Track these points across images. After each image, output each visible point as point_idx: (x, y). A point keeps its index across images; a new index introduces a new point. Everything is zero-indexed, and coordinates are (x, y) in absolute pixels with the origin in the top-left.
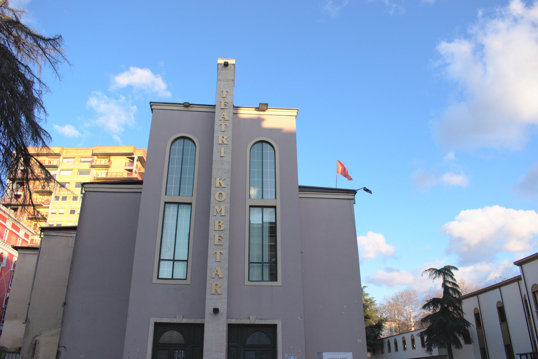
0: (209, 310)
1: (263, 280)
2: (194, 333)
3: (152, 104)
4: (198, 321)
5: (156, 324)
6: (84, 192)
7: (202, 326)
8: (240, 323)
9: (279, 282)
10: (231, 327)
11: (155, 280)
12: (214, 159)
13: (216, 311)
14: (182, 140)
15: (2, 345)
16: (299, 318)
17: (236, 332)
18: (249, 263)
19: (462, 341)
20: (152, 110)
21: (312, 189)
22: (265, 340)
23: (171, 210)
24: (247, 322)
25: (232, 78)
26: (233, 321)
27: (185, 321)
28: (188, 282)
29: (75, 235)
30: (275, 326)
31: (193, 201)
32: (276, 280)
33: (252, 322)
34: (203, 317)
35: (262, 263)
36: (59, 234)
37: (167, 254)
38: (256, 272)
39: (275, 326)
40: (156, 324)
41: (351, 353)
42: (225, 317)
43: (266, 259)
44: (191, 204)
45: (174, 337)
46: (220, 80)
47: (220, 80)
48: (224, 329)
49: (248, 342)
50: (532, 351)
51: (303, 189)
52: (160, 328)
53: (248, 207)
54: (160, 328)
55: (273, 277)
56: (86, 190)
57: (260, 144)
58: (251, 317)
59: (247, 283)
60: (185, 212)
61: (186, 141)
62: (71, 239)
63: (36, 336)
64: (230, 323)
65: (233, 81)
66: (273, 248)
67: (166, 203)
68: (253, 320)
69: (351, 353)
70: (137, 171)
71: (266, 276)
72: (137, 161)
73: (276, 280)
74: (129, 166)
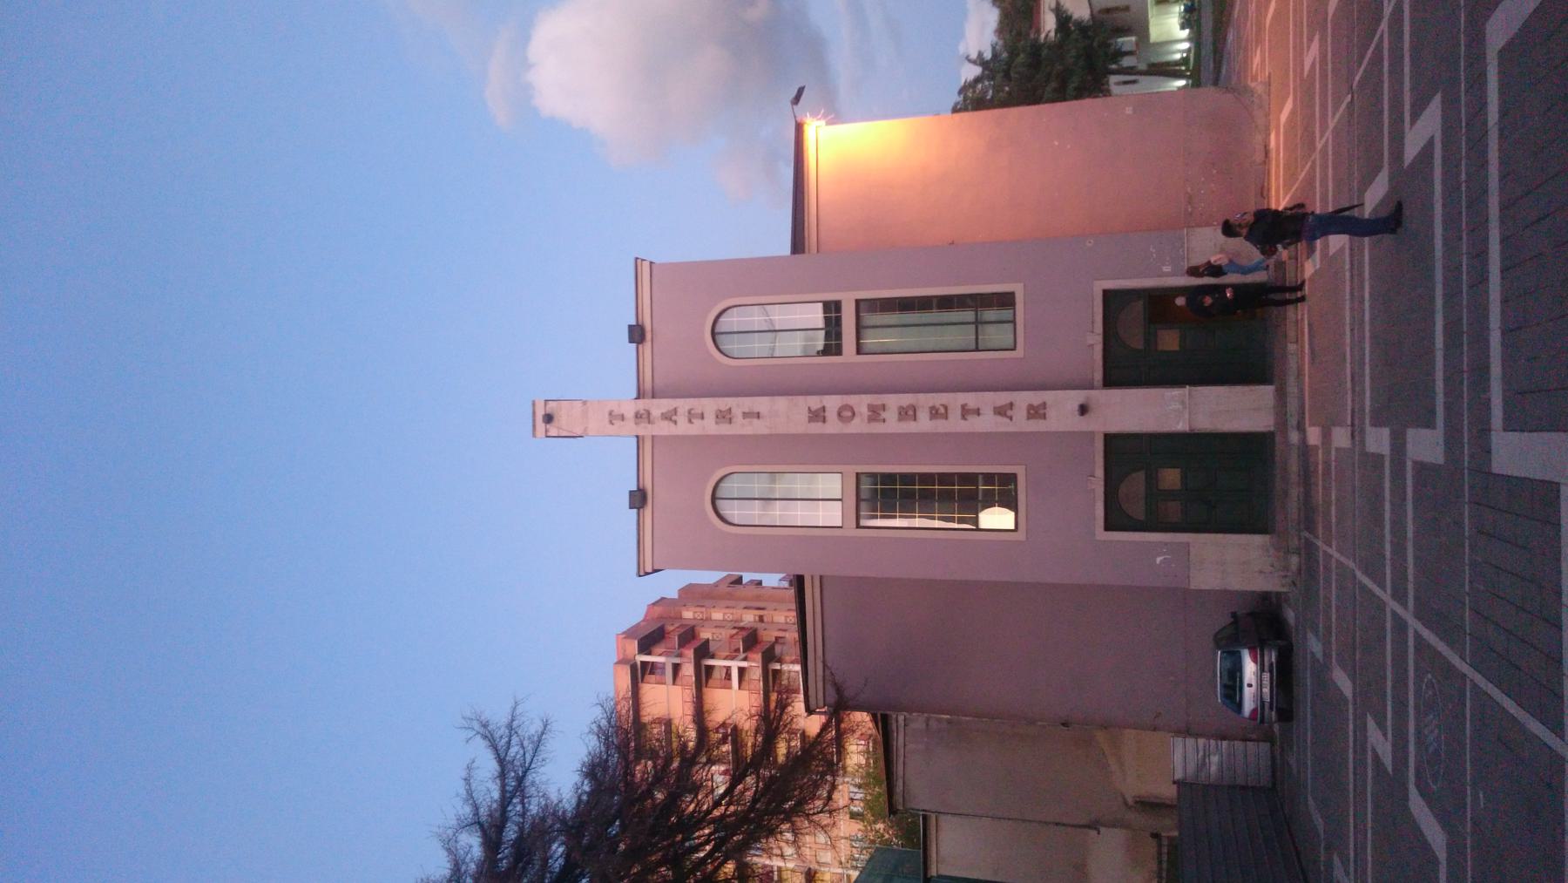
1: (1014, 322)
2: (1124, 453)
4: (1099, 445)
5: (1109, 527)
7: (1109, 439)
9: (1017, 289)
10: (1109, 382)
13: (1083, 409)
14: (720, 503)
17: (1123, 369)
18: (977, 350)
19: (1299, 294)
20: (655, 571)
24: (1099, 349)
25: (579, 404)
26: (1098, 376)
27: (1100, 472)
30: (1107, 294)
35: (977, 323)
36: (900, 773)
38: (996, 335)
39: (1107, 294)
40: (1109, 527)
41: (1441, 460)
43: (969, 315)
45: (1135, 484)
48: (1117, 394)
49: (1140, 346)
51: (798, 245)
52: (1116, 520)
54: (1116, 520)
55: (1006, 300)
57: (720, 338)
59: (1019, 353)
62: (911, 746)
63: (1126, 803)
65: (585, 403)
66: (946, 303)
68: (1096, 340)
69: (1441, 460)
70: (677, 651)
71: (1006, 314)
72: (649, 654)
74: (663, 673)
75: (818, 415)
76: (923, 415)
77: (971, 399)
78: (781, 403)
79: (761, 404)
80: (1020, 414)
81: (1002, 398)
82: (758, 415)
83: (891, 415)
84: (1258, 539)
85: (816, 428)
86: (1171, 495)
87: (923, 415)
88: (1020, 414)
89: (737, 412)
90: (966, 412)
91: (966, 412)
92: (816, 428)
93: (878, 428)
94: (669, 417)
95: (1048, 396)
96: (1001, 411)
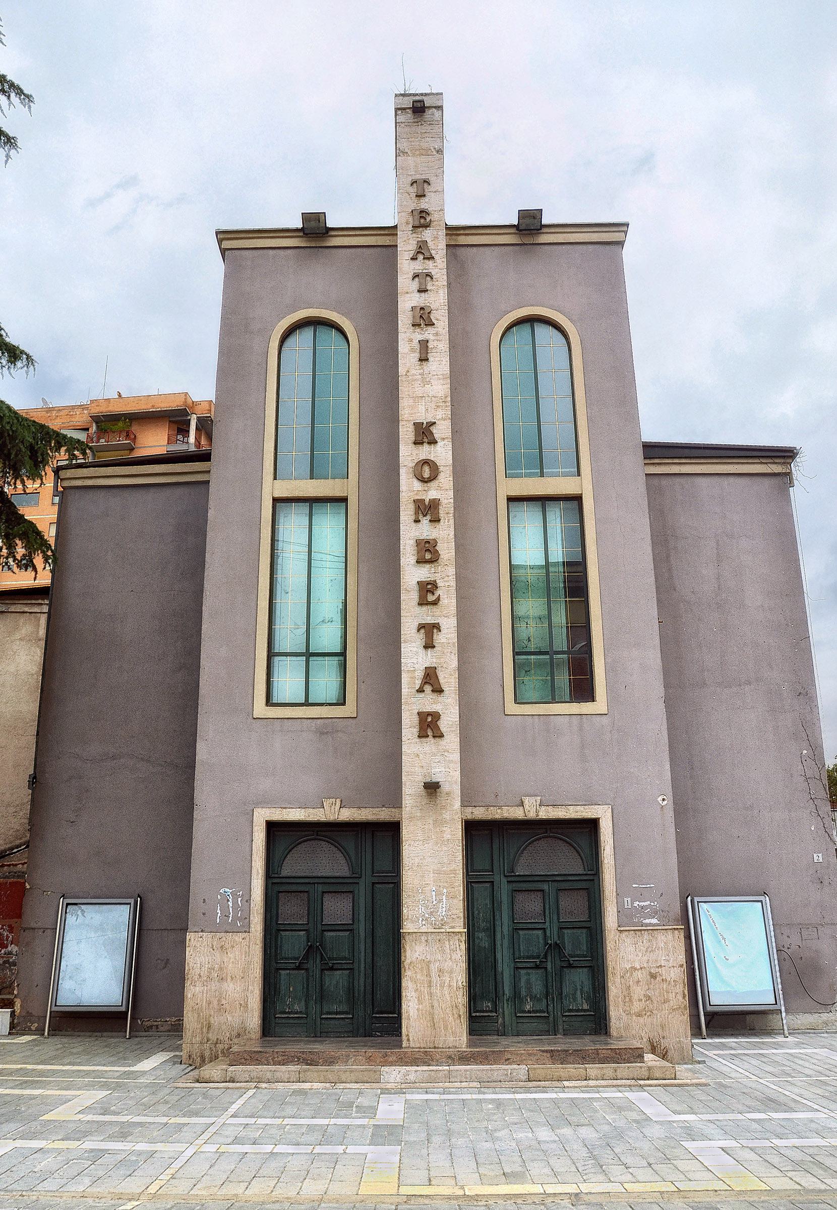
0: (411, 789)
3: (226, 244)
4: (383, 815)
5: (273, 827)
6: (60, 489)
7: (393, 829)
8: (498, 817)
9: (600, 705)
10: (471, 828)
11: (260, 708)
12: (402, 370)
13: (432, 788)
15: (3, 72)
16: (660, 798)
17: (486, 839)
21: (687, 452)
22: (566, 862)
23: (293, 526)
24: (517, 814)
26: (479, 813)
27: (346, 815)
28: (349, 710)
29: (45, 609)
30: (593, 825)
31: (348, 487)
32: (592, 698)
33: (532, 815)
34: (396, 800)
37: (289, 637)
39: (593, 825)
40: (273, 827)
42: (457, 804)
43: (561, 641)
44: (344, 500)
46: (405, 153)
47: (405, 153)
48: (455, 833)
50: (544, 222)
51: (655, 451)
53: (502, 503)
55: (583, 689)
56: (66, 484)
57: (526, 329)
58: (526, 800)
60: (330, 531)
61: (322, 331)
64: (469, 817)
67: (276, 500)
73: (592, 698)
75: (424, 434)
76: (424, 573)
77: (448, 635)
78: (440, 388)
79: (440, 363)
80: (428, 702)
81: (448, 679)
82: (423, 359)
83: (425, 530)
84: (254, 1020)
85: (406, 433)
86: (315, 911)
87: (424, 573)
88: (428, 702)
89: (428, 334)
90: (429, 630)
91: (429, 630)
92: (406, 433)
93: (406, 514)
94: (431, 679)
95: (452, 741)
96: (431, 679)
